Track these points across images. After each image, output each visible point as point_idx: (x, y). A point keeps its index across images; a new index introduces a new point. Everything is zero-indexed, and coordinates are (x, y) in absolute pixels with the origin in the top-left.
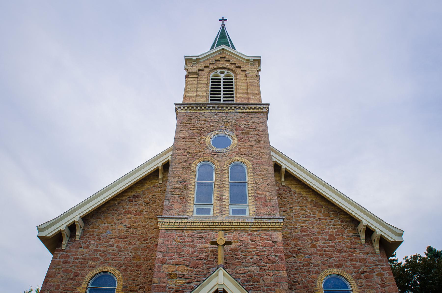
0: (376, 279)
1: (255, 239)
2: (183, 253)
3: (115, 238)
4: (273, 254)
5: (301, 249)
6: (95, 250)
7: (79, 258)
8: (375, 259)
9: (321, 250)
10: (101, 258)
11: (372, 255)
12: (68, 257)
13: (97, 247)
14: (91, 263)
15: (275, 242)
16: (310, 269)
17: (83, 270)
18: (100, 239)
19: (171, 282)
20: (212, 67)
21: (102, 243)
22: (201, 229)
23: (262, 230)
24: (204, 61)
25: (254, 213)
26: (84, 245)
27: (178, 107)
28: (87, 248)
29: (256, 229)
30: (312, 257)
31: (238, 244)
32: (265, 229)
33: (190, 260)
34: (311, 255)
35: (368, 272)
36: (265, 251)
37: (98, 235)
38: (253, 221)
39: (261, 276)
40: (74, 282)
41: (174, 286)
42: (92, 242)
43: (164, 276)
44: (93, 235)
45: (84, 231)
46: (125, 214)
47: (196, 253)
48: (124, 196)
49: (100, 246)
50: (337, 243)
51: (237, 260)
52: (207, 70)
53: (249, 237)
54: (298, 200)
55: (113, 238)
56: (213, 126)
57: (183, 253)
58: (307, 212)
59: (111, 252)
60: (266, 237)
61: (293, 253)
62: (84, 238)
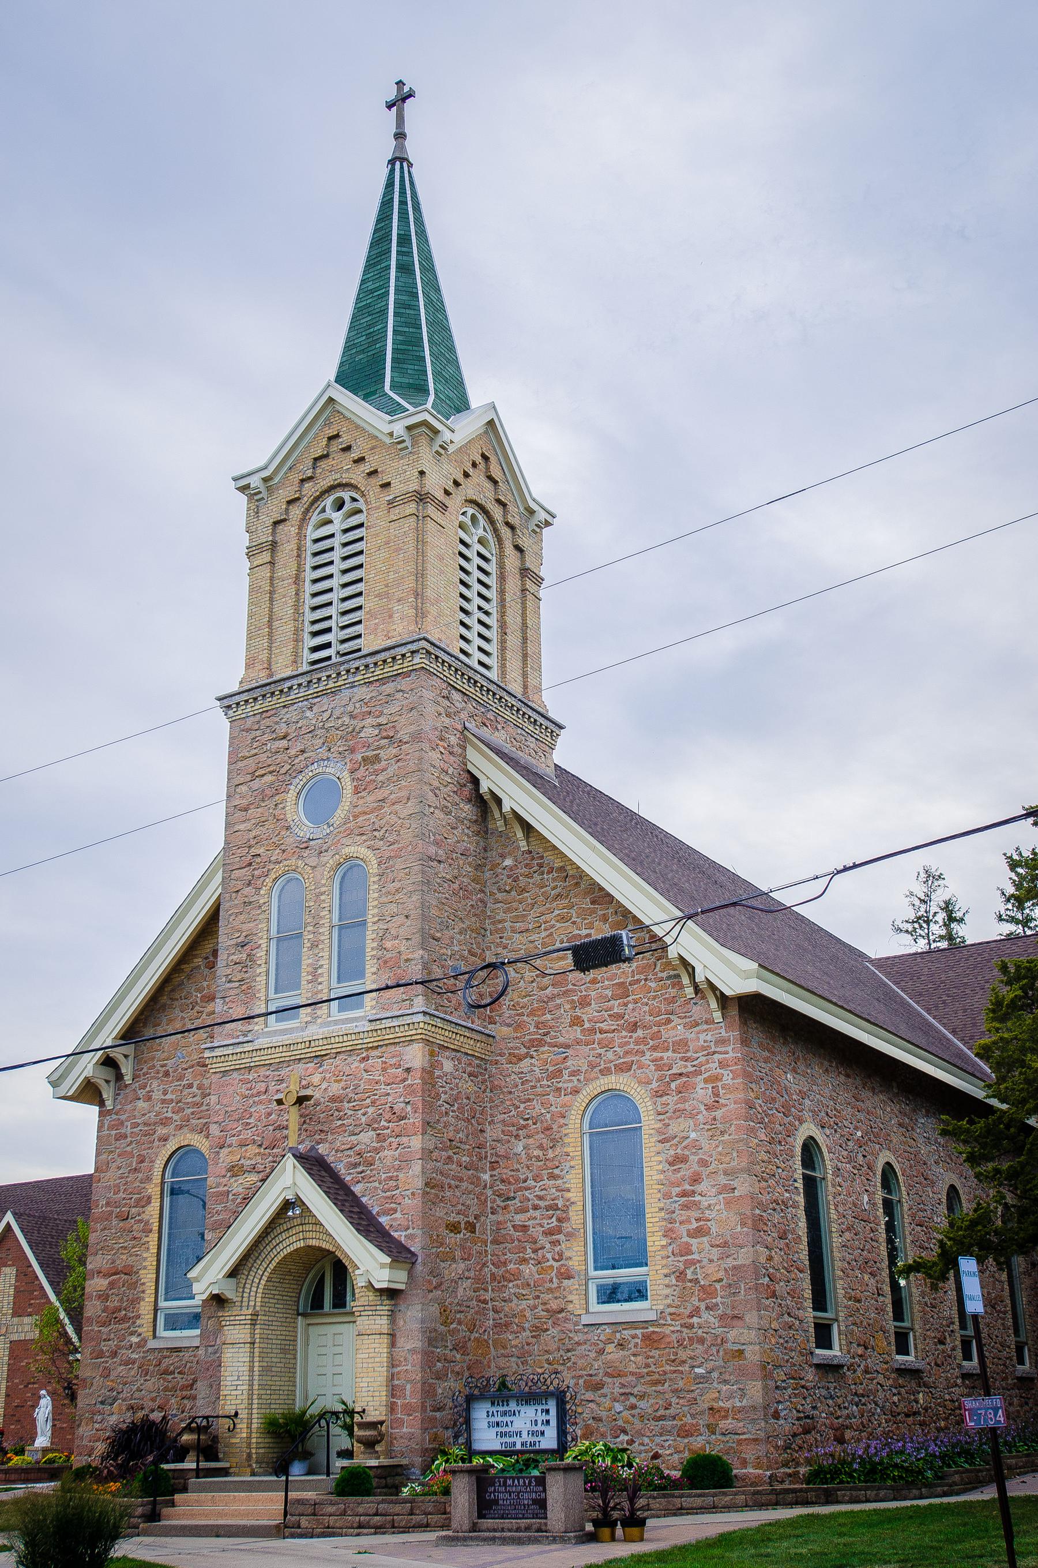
0: (702, 1091)
1: (373, 1069)
2: (251, 1121)
3: (193, 1066)
4: (402, 1099)
5: (548, 1033)
6: (163, 1101)
7: (139, 1125)
8: (709, 1038)
9: (592, 1031)
10: (175, 1117)
11: (705, 1027)
12: (122, 1123)
13: (165, 1093)
14: (161, 1131)
15: (408, 1070)
16: (560, 1085)
17: (149, 1148)
18: (167, 1074)
19: (236, 1181)
20: (310, 490)
21: (171, 1082)
22: (277, 1060)
23: (386, 1045)
24: (285, 477)
25: (374, 1002)
26: (144, 1092)
27: (228, 702)
28: (149, 1098)
29: (375, 1044)
30: (570, 1052)
31: (343, 1084)
32: (391, 1041)
33: (263, 1132)
34: (568, 1047)
35: (687, 1075)
36: (388, 1094)
37: (162, 1066)
38: (368, 1027)
39: (377, 1151)
40: (140, 1175)
41: (240, 1189)
42: (155, 1083)
43: (223, 1173)
44: (154, 1066)
45: (138, 1059)
46: (204, 1004)
47: (273, 1116)
48: (196, 956)
49: (170, 1090)
50: (630, 1006)
51: (340, 1122)
52: (296, 511)
53: (362, 1065)
54: (558, 890)
55: (190, 1067)
56: (303, 751)
57: (251, 1121)
58: (574, 923)
59: (190, 1100)
60: (393, 1061)
61: (529, 1048)
62: (139, 1076)
